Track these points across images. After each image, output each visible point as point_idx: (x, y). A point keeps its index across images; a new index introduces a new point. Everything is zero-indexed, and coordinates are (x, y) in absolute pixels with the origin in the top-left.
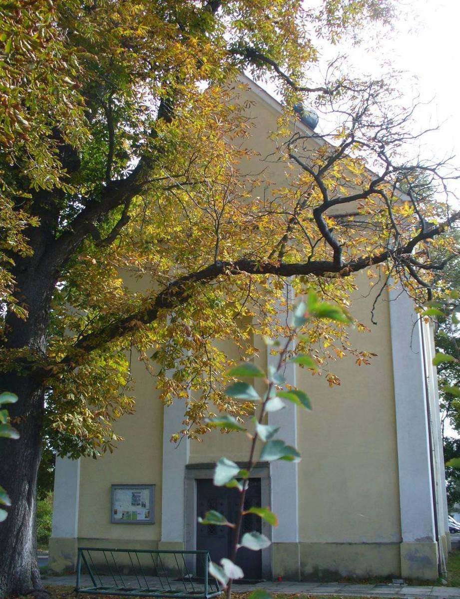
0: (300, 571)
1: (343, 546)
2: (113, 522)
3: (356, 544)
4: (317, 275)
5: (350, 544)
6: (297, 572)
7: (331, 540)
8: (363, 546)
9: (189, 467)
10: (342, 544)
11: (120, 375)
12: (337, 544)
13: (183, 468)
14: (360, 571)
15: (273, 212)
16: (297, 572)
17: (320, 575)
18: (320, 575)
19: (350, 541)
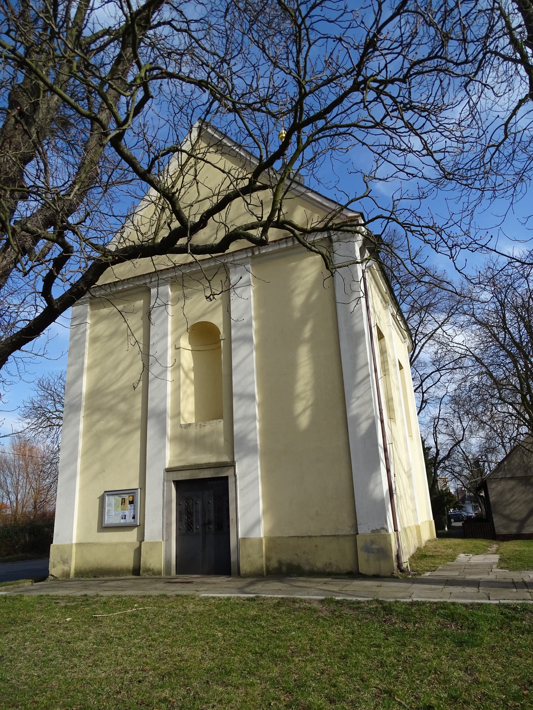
0: (264, 566)
1: (304, 539)
2: (103, 528)
3: (316, 536)
4: (359, 425)
5: (310, 537)
6: (262, 568)
7: (292, 534)
8: (322, 538)
9: (168, 471)
10: (303, 537)
11: (361, 79)
12: (298, 537)
13: (162, 473)
14: (319, 565)
15: (103, 195)
16: (262, 568)
17: (284, 568)
18: (284, 568)
19: (310, 534)
